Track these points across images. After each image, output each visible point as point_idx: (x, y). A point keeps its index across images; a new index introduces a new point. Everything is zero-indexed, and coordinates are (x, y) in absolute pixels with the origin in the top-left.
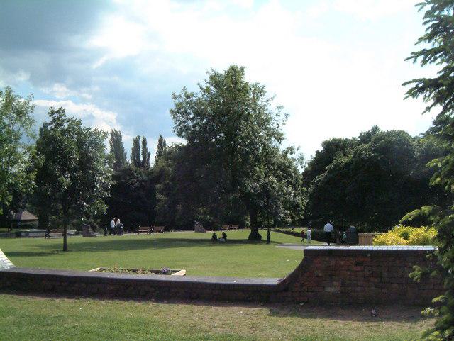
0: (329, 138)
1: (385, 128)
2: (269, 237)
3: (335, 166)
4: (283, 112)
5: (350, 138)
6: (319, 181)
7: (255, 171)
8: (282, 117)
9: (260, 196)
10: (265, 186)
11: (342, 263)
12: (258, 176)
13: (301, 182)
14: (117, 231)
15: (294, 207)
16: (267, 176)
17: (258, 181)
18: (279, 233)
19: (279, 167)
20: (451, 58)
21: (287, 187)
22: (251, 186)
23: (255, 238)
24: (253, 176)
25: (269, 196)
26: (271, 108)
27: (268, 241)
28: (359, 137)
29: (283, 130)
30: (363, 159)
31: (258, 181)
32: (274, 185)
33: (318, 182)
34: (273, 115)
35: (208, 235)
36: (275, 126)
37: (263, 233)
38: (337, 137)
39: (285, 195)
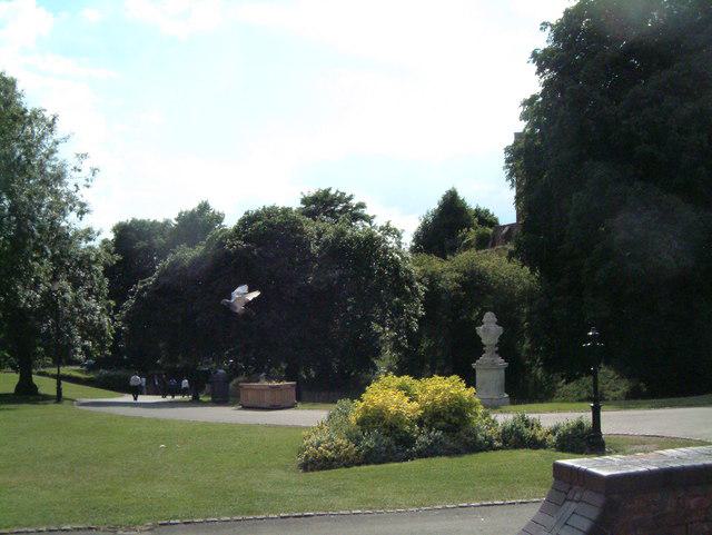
0: (126, 218)
1: (139, 218)
2: (59, 390)
3: (173, 264)
4: (86, 166)
5: (161, 220)
6: (145, 289)
7: (32, 269)
8: (86, 172)
9: (40, 315)
10: (47, 295)
11: (692, 503)
12: (37, 279)
13: (106, 291)
14: (136, 391)
15: (94, 332)
16: (55, 279)
17: (35, 287)
18: (44, 378)
19: (80, 264)
20: (6, 157)
21: (87, 299)
22: (28, 297)
23: (26, 393)
24: (29, 277)
25: (56, 313)
26: (65, 155)
27: (59, 398)
28: (177, 220)
29: (84, 195)
30: (227, 254)
31: (35, 287)
32: (66, 295)
33: (142, 291)
34: (68, 169)
35: (158, 399)
36: (72, 188)
37: (45, 385)
38: (139, 218)
39: (83, 312)
